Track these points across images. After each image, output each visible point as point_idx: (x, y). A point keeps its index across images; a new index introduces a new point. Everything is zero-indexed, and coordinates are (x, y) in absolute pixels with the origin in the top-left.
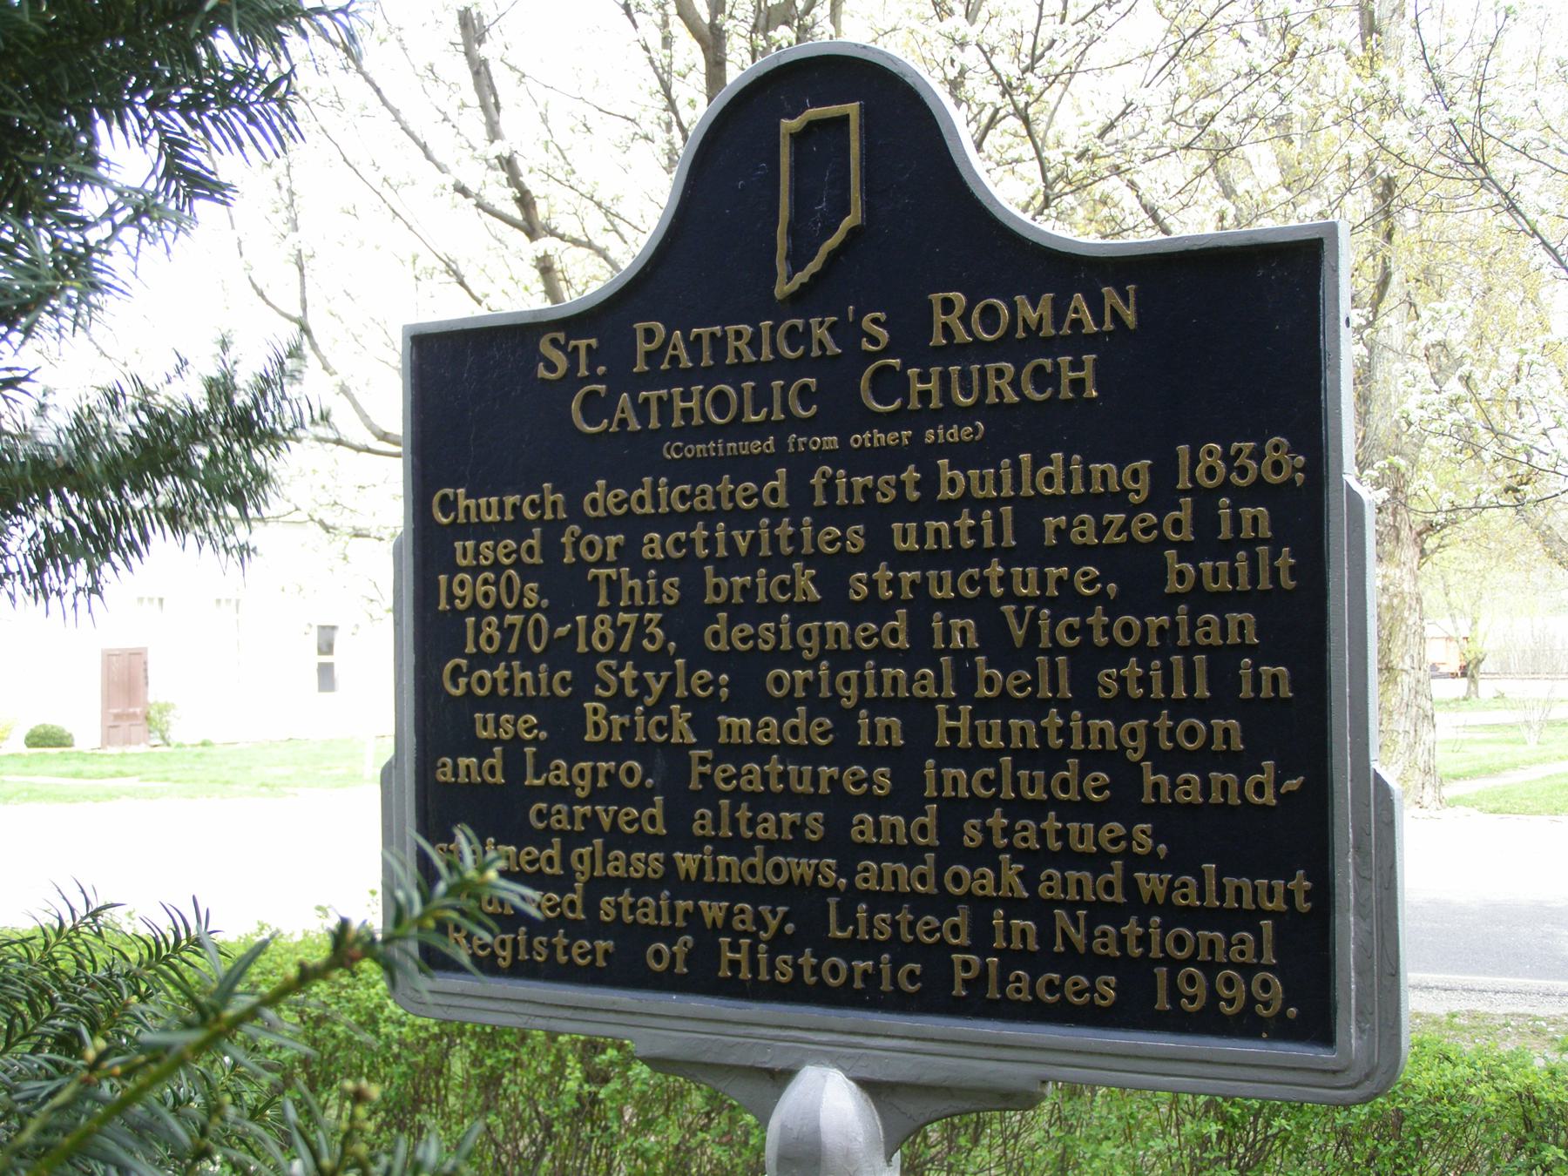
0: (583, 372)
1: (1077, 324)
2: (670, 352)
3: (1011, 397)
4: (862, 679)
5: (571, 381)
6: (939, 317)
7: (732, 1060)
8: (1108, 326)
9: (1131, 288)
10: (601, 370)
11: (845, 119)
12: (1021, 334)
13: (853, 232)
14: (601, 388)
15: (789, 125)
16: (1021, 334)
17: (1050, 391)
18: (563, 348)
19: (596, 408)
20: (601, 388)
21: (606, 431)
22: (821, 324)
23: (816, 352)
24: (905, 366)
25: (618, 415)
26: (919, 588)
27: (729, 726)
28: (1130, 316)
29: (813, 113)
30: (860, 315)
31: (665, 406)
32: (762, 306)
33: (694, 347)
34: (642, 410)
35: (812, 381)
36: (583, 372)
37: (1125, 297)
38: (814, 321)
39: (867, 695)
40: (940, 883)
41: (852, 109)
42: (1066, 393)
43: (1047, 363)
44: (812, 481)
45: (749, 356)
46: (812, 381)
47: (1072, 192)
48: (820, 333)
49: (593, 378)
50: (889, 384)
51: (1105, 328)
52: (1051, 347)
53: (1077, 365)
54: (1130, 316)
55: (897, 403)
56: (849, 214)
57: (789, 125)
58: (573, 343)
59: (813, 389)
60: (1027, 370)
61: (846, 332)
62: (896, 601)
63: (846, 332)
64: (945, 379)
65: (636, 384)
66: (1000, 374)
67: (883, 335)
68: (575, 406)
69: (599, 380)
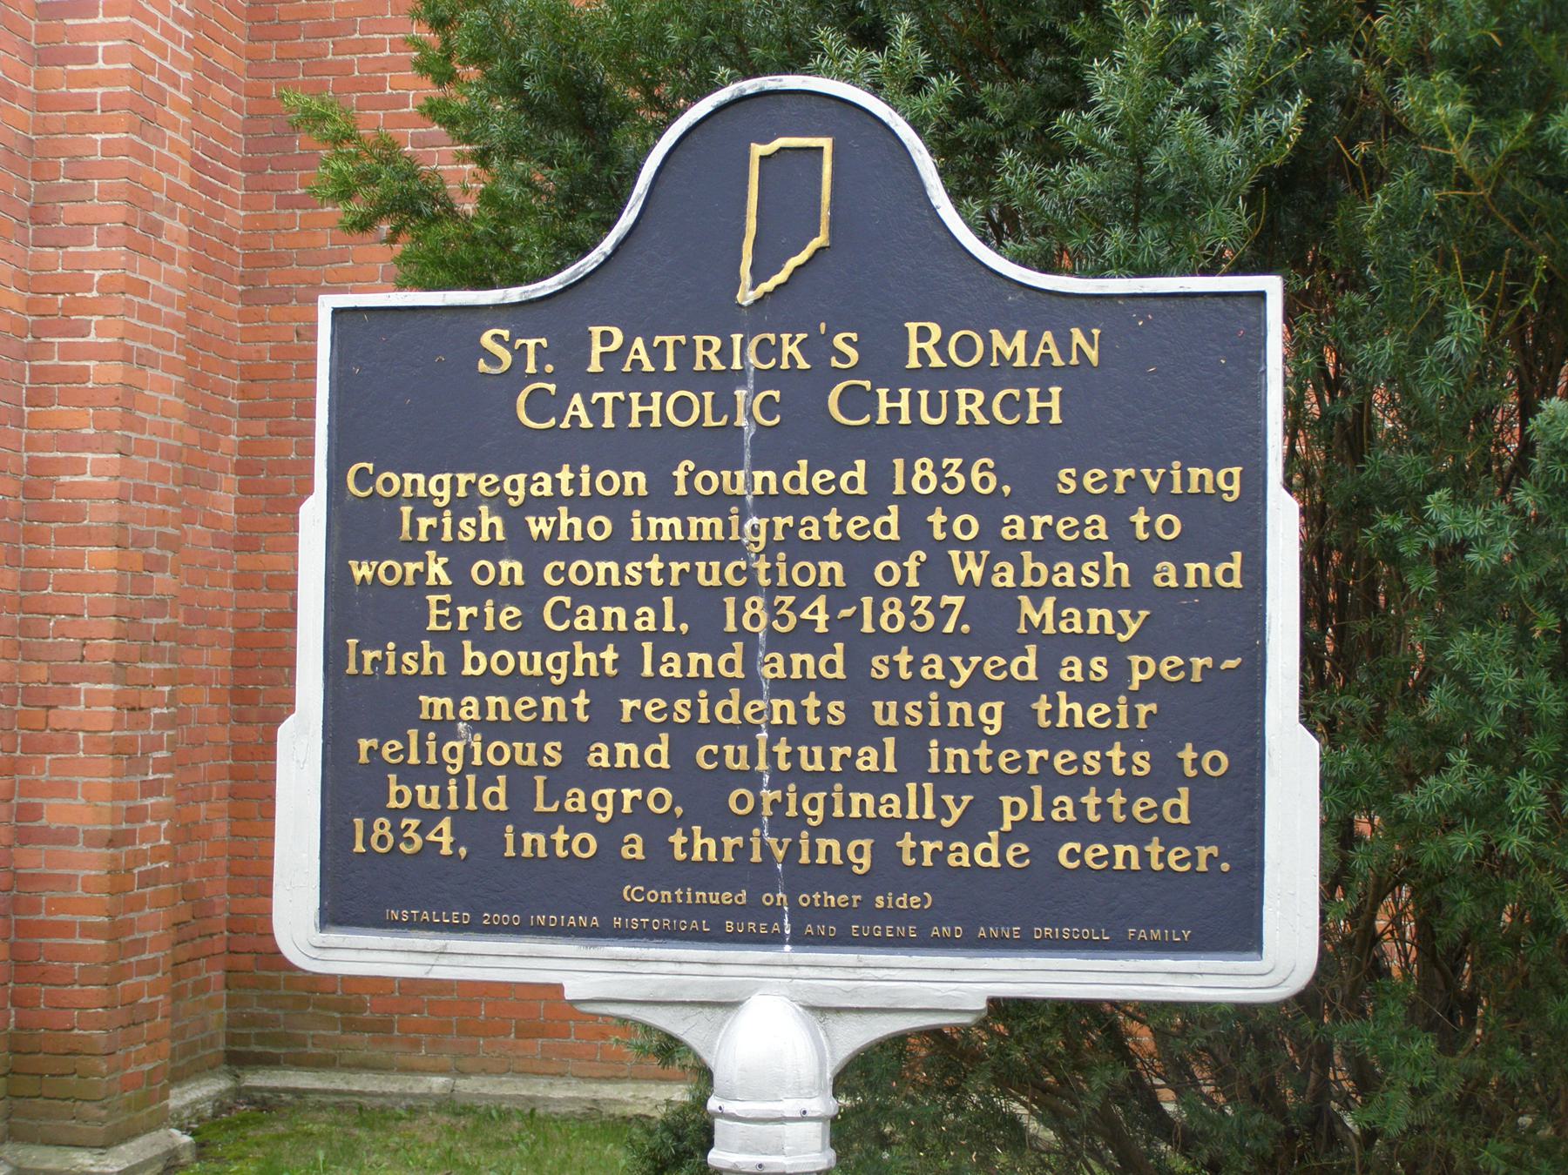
0: (531, 368)
1: (1046, 358)
2: (632, 356)
3: (981, 420)
4: (571, 659)
5: (516, 376)
6: (914, 345)
7: (900, 1006)
8: (1074, 361)
9: (1096, 332)
10: (549, 368)
11: (1261, 295)
12: (994, 363)
13: (819, 251)
14: (552, 388)
15: (758, 150)
16: (994, 363)
17: (774, 361)
18: (509, 345)
19: (539, 403)
20: (552, 388)
21: (556, 426)
22: (791, 341)
23: (785, 365)
24: (874, 387)
25: (570, 412)
26: (688, 577)
27: (431, 705)
28: (1093, 355)
29: (781, 142)
30: (831, 333)
31: (622, 408)
32: (726, 318)
33: (657, 354)
34: (596, 410)
35: (776, 394)
36: (531, 368)
37: (1090, 339)
38: (786, 337)
39: (575, 674)
40: (1002, 857)
41: (826, 143)
42: (1033, 418)
43: (772, 337)
44: (675, 473)
45: (717, 365)
46: (776, 394)
47: (989, 217)
48: (789, 349)
49: (540, 376)
50: (856, 401)
51: (1072, 362)
52: (1023, 377)
53: (1044, 396)
54: (1093, 355)
55: (867, 419)
56: (818, 235)
57: (758, 150)
58: (520, 342)
59: (778, 400)
60: (756, 341)
61: (817, 348)
62: (666, 589)
63: (817, 348)
64: (914, 401)
65: (590, 384)
66: (970, 399)
67: (854, 355)
68: (522, 399)
69: (548, 378)
